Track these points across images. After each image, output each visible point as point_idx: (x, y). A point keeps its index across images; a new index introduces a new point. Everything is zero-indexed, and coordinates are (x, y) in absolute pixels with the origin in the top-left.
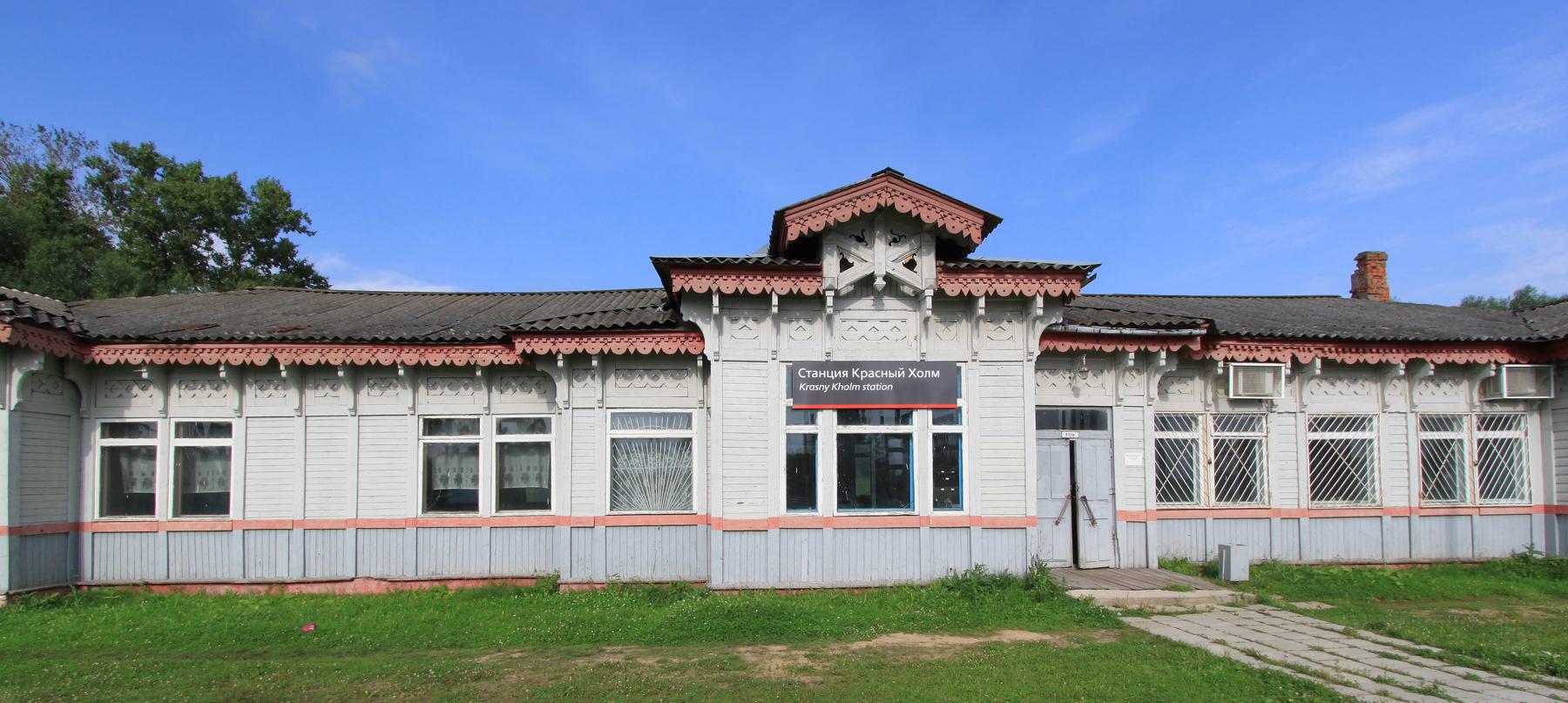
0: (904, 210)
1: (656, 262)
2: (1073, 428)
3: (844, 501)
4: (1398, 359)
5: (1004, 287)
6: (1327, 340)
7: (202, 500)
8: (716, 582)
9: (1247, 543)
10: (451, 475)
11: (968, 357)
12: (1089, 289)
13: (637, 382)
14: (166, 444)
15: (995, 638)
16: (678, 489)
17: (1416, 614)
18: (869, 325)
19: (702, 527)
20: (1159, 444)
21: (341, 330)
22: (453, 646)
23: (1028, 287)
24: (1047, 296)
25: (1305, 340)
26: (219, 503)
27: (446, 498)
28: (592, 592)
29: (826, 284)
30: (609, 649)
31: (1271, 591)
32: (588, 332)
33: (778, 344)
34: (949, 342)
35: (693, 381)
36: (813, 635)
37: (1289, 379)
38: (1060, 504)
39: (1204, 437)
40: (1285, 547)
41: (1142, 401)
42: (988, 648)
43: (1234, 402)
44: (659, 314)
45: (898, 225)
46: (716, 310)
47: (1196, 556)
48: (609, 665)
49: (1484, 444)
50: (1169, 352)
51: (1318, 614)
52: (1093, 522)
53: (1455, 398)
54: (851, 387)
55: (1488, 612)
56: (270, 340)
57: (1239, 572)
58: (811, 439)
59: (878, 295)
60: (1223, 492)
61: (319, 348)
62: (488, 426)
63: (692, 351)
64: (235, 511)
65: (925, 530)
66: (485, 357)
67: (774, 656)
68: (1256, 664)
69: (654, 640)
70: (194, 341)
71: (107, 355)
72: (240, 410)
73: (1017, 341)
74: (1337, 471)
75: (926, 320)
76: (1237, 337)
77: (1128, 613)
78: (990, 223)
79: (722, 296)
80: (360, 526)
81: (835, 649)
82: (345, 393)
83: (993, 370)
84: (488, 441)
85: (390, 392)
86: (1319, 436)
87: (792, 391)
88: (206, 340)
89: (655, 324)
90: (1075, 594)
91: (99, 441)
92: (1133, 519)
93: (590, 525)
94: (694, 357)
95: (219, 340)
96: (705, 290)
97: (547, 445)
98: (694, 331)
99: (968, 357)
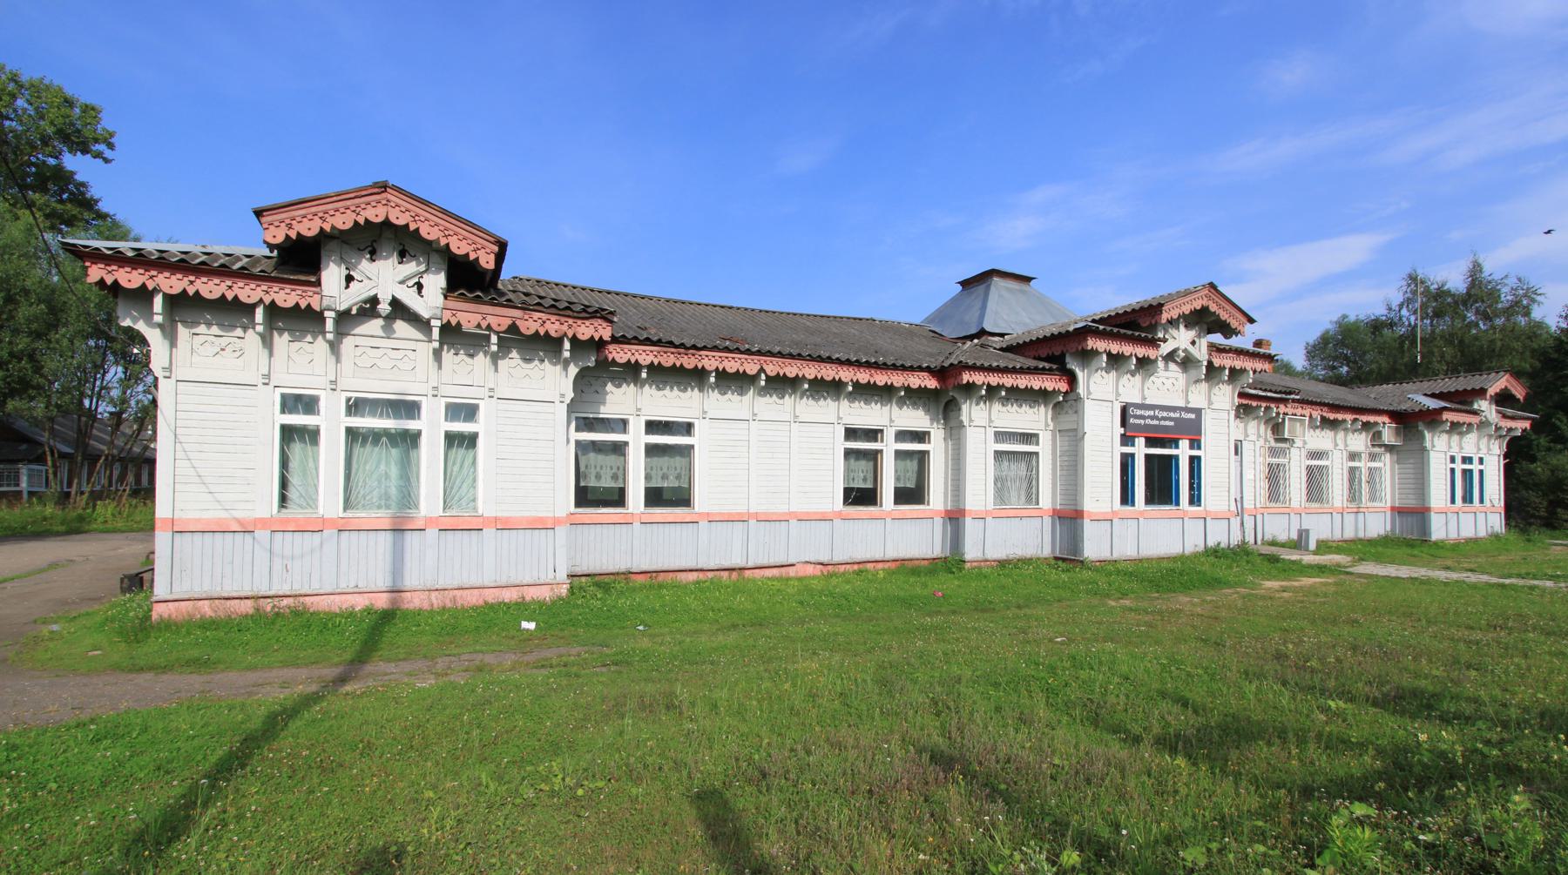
4: (1349, 417)
14: (637, 439)
20: (1309, 468)
26: (682, 498)
45: (406, 242)
61: (799, 363)
62: (890, 435)
74: (1315, 481)
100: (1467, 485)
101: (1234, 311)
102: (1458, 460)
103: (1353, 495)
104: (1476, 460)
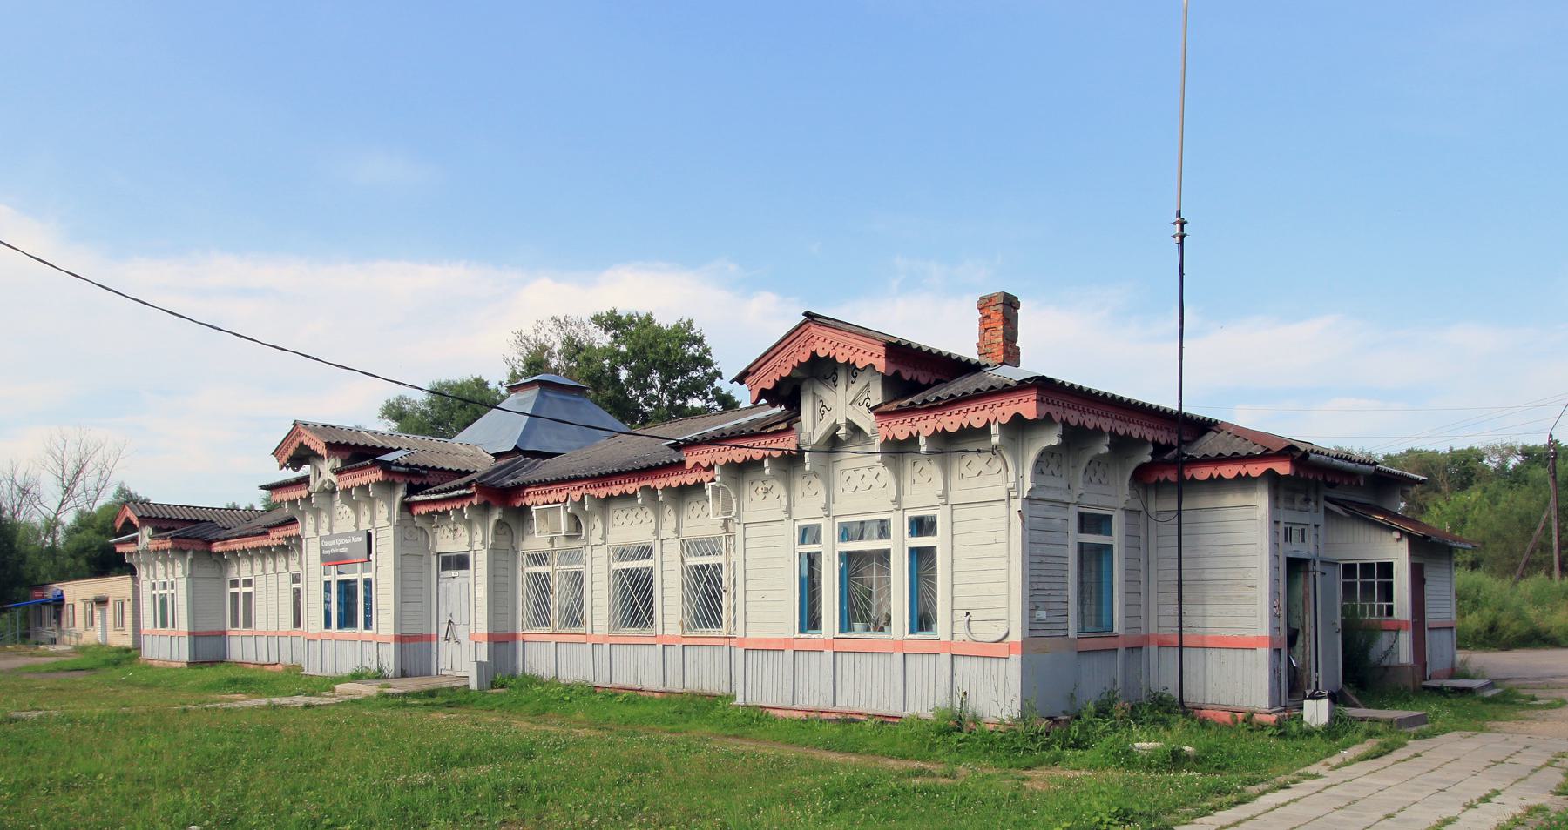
102: (829, 532)
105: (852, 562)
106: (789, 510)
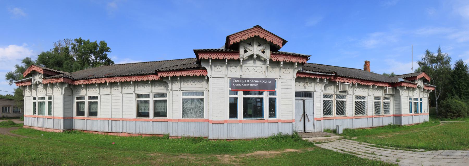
0: (262, 37)
1: (195, 51)
2: (305, 97)
3: (245, 116)
4: (371, 84)
5: (288, 59)
6: (358, 79)
7: (93, 113)
8: (210, 137)
9: (343, 124)
10: (143, 108)
11: (278, 78)
12: (308, 62)
13: (189, 83)
14: (86, 101)
15: (284, 151)
16: (200, 112)
17: (373, 138)
18: (252, 68)
19: (206, 123)
20: (324, 101)
21: (119, 74)
22: (144, 151)
23: (294, 60)
24: (298, 63)
25: (354, 78)
27: (142, 114)
28: (178, 139)
29: (241, 56)
30: (183, 154)
31: (347, 135)
32: (177, 70)
33: (227, 73)
34: (273, 74)
35: (204, 83)
36: (236, 152)
37: (351, 87)
38: (301, 116)
39: (334, 100)
40: (351, 125)
41: (320, 91)
42: (283, 154)
43: (340, 92)
44: (195, 65)
46: (210, 64)
47: (332, 128)
48: (183, 159)
49: (384, 102)
50: (327, 79)
51: (355, 140)
52: (309, 121)
53: (380, 93)
54: (247, 85)
55: (384, 136)
56: (105, 77)
57: (341, 132)
58: (236, 99)
59: (255, 60)
60: (338, 113)
62: (151, 95)
63: (204, 75)
64: (98, 116)
65: (266, 123)
66: (151, 78)
67: (226, 158)
68: (343, 152)
69: (194, 152)
70: (91, 79)
71: (77, 83)
72: (99, 93)
73: (291, 74)
74: (360, 108)
75: (267, 67)
76: (341, 77)
77: (316, 143)
78: (284, 42)
79: (212, 60)
80: (123, 120)
81: (242, 155)
82: (120, 88)
83: (284, 81)
84: (151, 100)
85: (129, 88)
86: (357, 100)
87: (231, 86)
88: (93, 78)
89: (194, 68)
90: (304, 139)
91: (76, 101)
92: (318, 120)
93: (177, 121)
94: (205, 77)
95: (96, 78)
96: (207, 58)
97: (166, 100)
98: (205, 69)
99: (278, 77)
100: (416, 107)
101: (274, 37)
102: (413, 99)
103: (377, 110)
104: (47, 98)
105: (40, 103)
106: (31, 95)
